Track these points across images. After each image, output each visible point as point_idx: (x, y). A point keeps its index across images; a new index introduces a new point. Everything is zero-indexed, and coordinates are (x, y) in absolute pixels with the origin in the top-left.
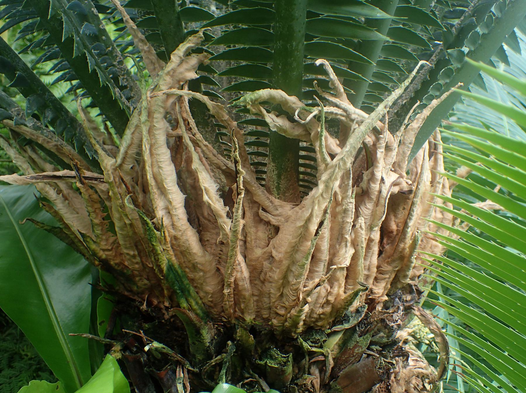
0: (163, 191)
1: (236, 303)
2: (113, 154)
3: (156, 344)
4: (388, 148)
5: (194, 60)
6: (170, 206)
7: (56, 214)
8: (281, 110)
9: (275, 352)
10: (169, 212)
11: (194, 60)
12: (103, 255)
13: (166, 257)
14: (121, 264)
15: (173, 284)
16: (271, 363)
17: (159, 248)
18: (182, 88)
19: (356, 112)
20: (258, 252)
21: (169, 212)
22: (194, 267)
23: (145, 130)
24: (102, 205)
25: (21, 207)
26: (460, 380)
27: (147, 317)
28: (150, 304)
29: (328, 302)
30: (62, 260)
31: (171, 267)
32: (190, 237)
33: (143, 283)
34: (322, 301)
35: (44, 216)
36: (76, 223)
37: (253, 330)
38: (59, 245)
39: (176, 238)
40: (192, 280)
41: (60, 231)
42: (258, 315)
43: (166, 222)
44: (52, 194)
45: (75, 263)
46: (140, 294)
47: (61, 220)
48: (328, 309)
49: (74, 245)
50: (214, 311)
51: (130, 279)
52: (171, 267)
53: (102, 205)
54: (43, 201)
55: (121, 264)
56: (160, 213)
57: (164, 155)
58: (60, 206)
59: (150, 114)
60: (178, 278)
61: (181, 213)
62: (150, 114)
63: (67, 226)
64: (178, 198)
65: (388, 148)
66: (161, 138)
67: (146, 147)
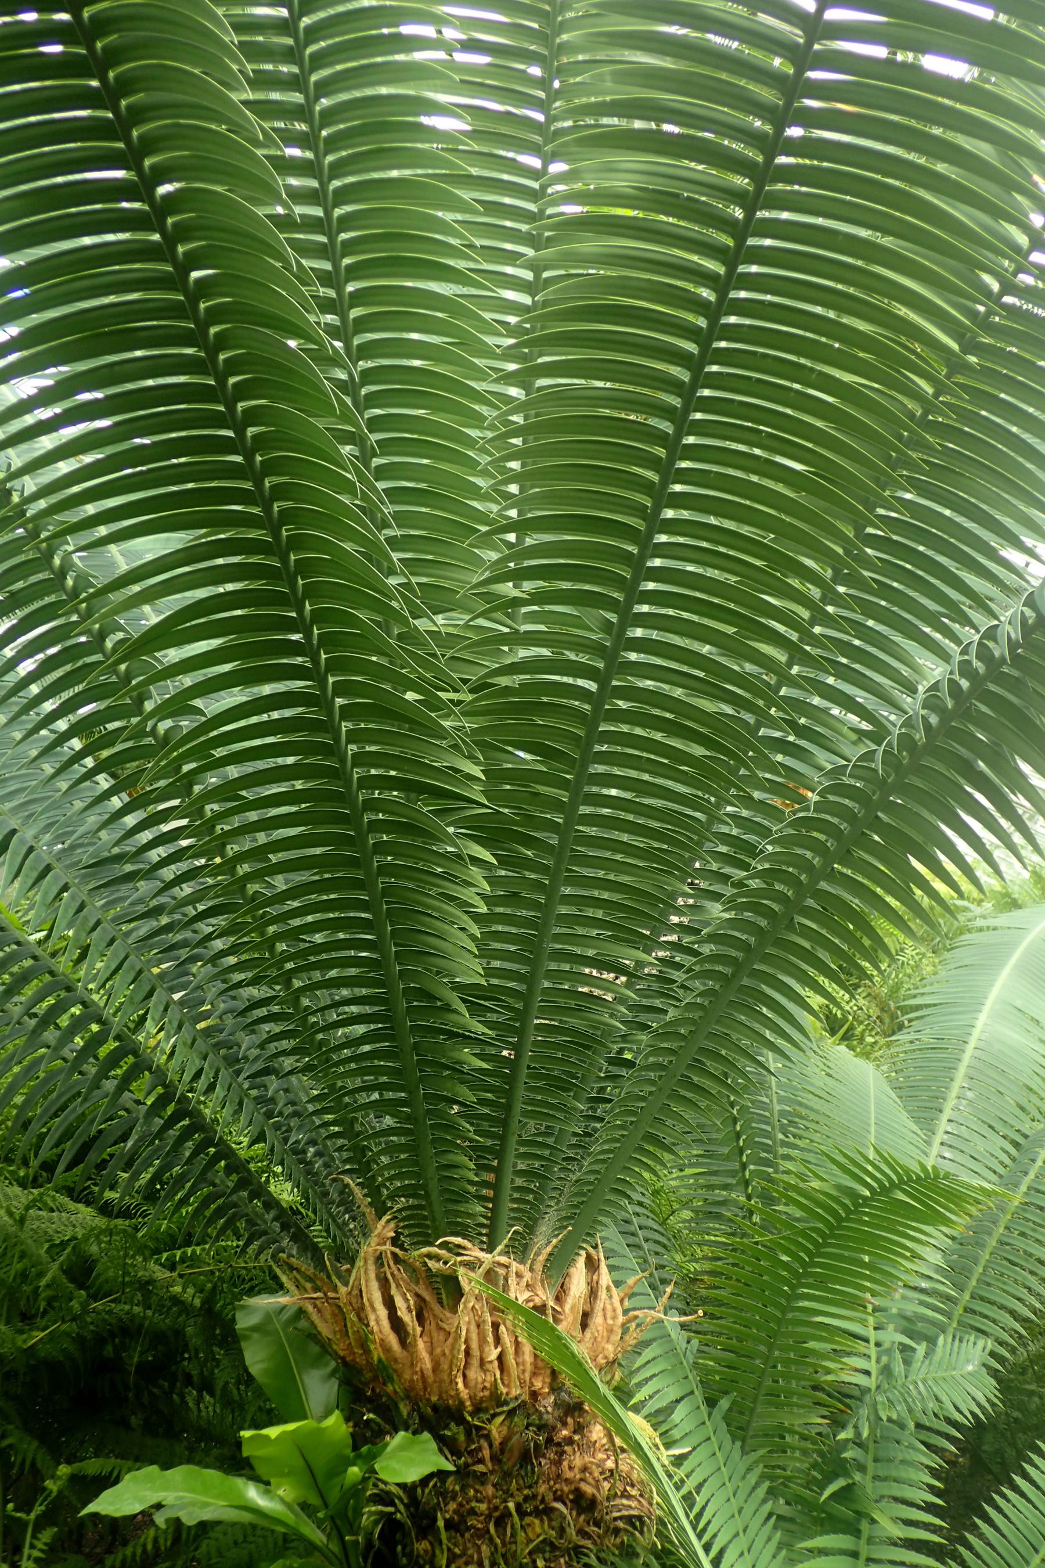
0: (374, 1309)
1: (425, 1389)
2: (346, 1284)
3: (371, 1416)
4: (519, 1275)
5: (392, 1225)
6: (379, 1317)
7: (312, 1323)
8: (437, 1258)
9: (453, 1426)
10: (377, 1321)
11: (392, 1225)
12: (342, 1353)
13: (377, 1353)
14: (354, 1360)
15: (384, 1372)
16: (448, 1433)
17: (372, 1347)
18: (385, 1244)
19: (482, 1255)
20: (438, 1351)
21: (377, 1321)
22: (396, 1360)
23: (362, 1271)
24: (339, 1314)
25: (286, 1316)
26: (69, 1250)
27: (370, 1400)
28: (373, 1390)
29: (484, 1388)
30: (316, 1362)
31: (380, 1360)
32: (393, 1340)
33: (368, 1375)
34: (480, 1386)
35: (303, 1324)
36: (325, 1330)
37: (435, 1408)
38: (315, 1349)
39: (382, 1340)
40: (395, 1371)
41: (314, 1336)
42: (440, 1398)
43: (376, 1329)
44: (310, 1308)
45: (327, 1365)
46: (367, 1384)
47: (316, 1328)
48: (487, 1393)
49: (325, 1348)
50: (412, 1394)
51: (360, 1372)
52: (380, 1360)
53: (339, 1314)
54: (301, 1312)
55: (354, 1360)
56: (372, 1323)
57: (374, 1285)
58: (315, 1317)
59: (366, 1261)
60: (385, 1368)
61: (385, 1323)
62: (366, 1261)
63: (320, 1333)
64: (383, 1312)
65: (519, 1275)
66: (372, 1275)
67: (363, 1282)
